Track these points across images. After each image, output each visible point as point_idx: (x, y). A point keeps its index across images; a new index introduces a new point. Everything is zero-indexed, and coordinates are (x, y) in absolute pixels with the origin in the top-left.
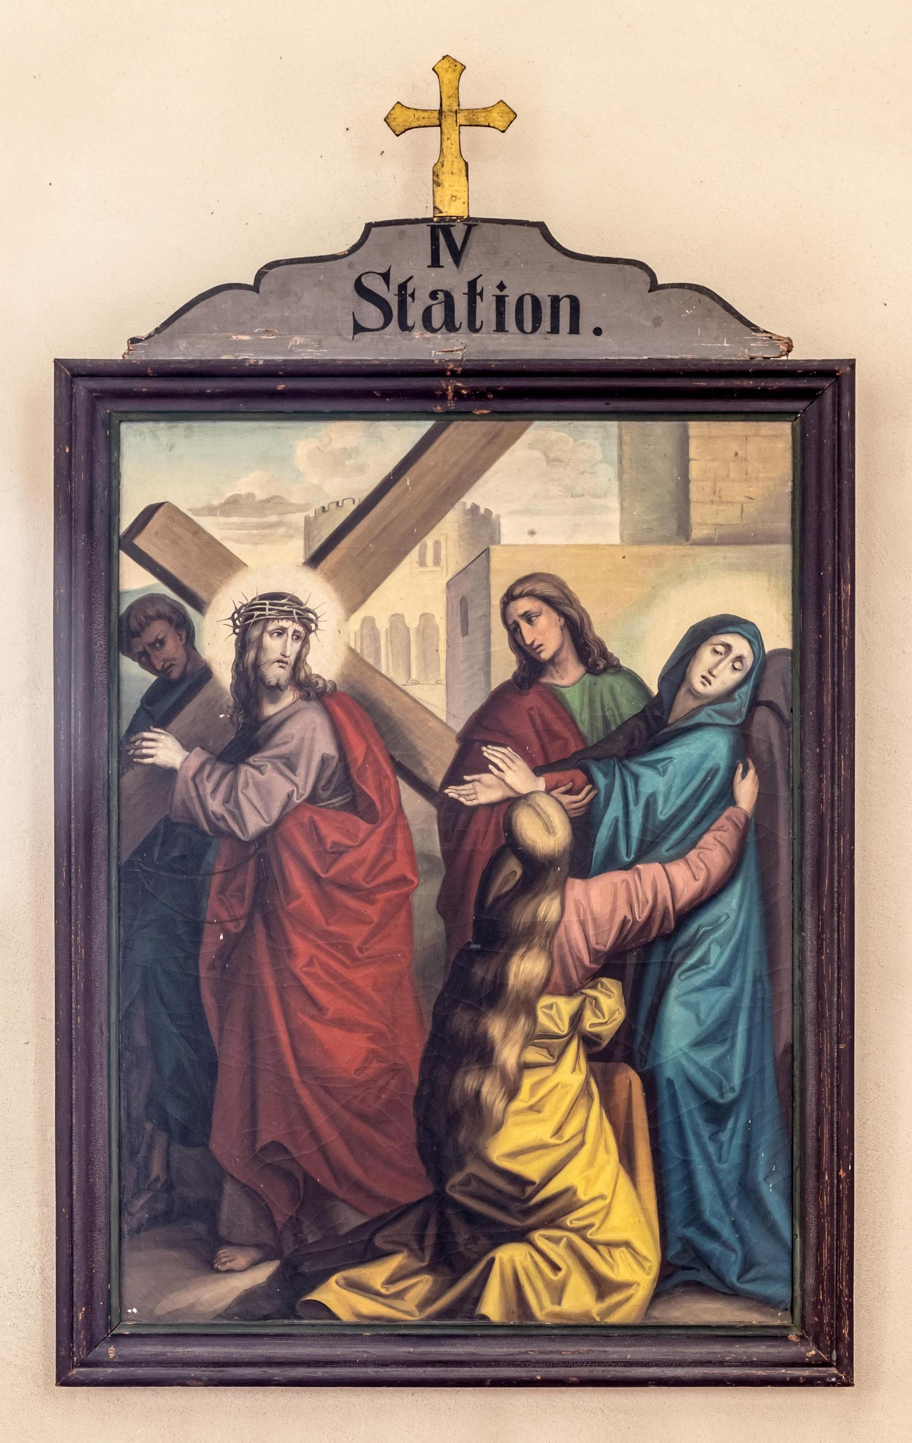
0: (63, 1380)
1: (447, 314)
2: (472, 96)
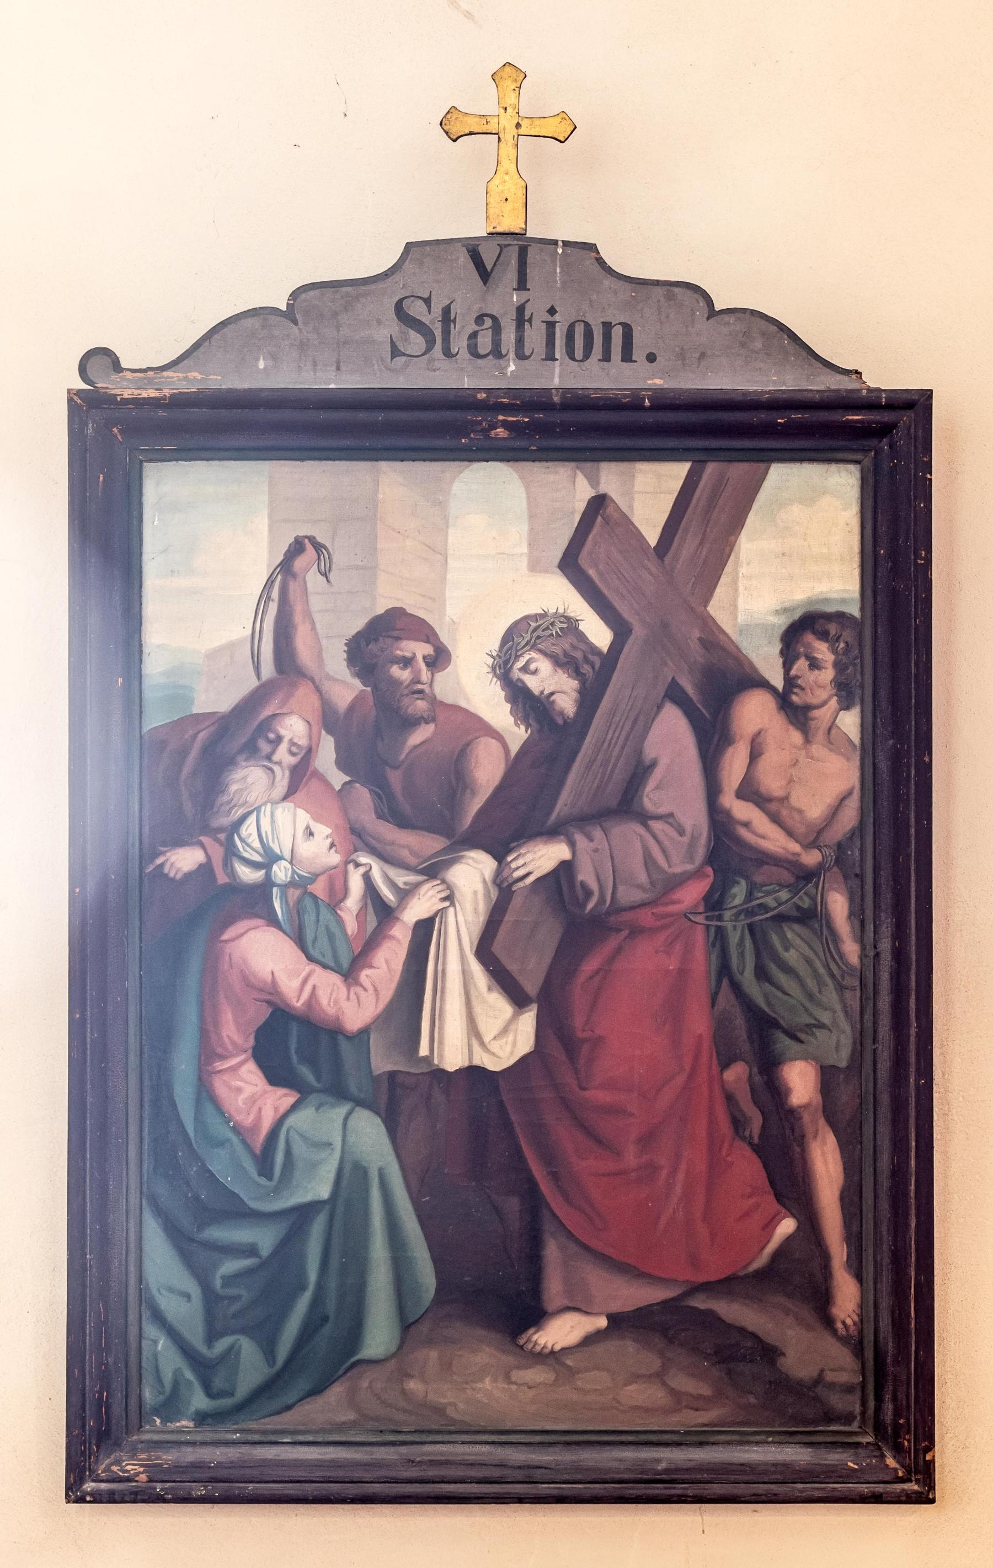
0: (75, 1492)
1: (489, 341)
2: (537, 98)
